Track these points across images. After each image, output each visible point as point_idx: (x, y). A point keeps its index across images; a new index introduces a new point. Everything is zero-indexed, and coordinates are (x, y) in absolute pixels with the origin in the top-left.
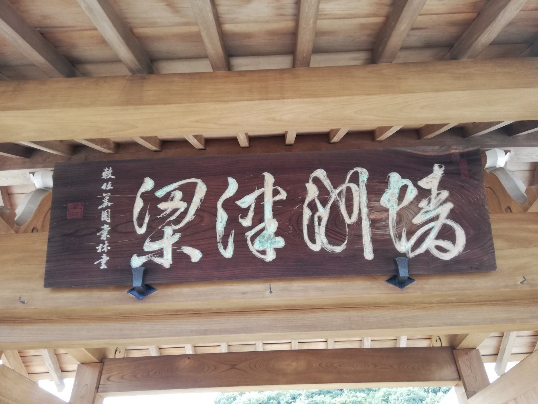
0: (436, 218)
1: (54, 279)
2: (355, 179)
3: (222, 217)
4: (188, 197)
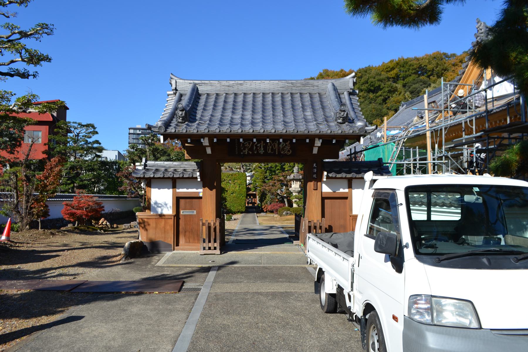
3: (255, 147)
4: (249, 144)
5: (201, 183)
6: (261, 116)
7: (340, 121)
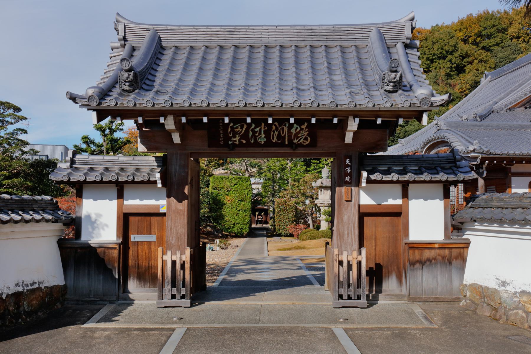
0: (304, 135)
1: (210, 146)
2: (285, 125)
4: (242, 128)
5: (164, 191)
6: (260, 81)
7: (390, 88)
